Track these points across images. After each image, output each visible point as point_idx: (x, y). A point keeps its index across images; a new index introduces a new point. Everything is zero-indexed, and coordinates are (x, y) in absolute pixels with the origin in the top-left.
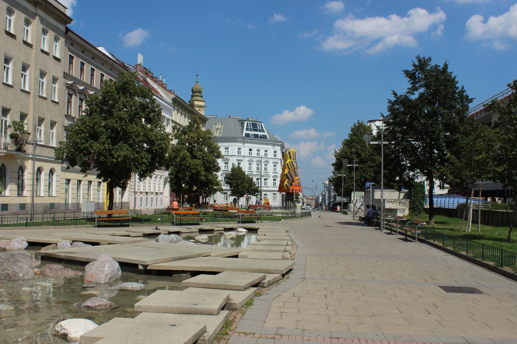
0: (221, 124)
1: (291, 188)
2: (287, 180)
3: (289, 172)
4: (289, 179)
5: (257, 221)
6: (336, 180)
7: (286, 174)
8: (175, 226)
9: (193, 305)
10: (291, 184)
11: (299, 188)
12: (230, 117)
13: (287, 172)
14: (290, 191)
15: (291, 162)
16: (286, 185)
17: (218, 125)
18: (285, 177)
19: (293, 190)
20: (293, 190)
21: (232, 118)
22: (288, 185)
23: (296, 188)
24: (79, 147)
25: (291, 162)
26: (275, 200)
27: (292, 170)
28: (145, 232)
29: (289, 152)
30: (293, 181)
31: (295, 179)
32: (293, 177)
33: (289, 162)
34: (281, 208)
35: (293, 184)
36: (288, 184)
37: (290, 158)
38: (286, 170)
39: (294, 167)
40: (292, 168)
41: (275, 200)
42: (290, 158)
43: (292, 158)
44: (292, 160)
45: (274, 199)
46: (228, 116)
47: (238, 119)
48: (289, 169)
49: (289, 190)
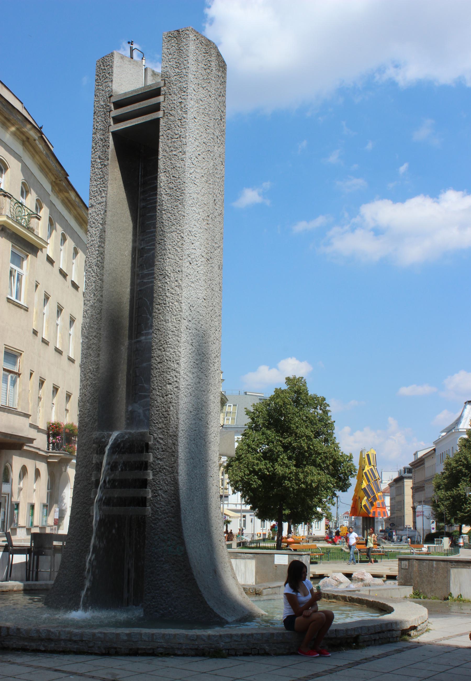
0: (234, 405)
1: (372, 511)
2: (366, 498)
3: (369, 486)
4: (369, 496)
5: (379, 560)
6: (451, 500)
7: (365, 488)
8: (359, 563)
9: (429, 651)
10: (372, 504)
11: (383, 510)
12: (246, 393)
13: (366, 485)
14: (371, 515)
15: (371, 469)
16: (365, 506)
17: (229, 406)
18: (362, 493)
19: (374, 512)
20: (374, 512)
21: (249, 395)
22: (368, 506)
23: (378, 510)
24: (254, 469)
25: (371, 469)
26: (318, 527)
27: (373, 482)
28: (315, 572)
29: (368, 455)
30: (375, 499)
31: (377, 496)
32: (374, 493)
33: (368, 470)
34: (325, 540)
35: (374, 503)
36: (368, 503)
37: (370, 463)
38: (364, 482)
39: (375, 477)
40: (372, 480)
41: (318, 527)
42: (370, 463)
43: (372, 465)
44: (372, 467)
45: (317, 527)
46: (242, 393)
47: (259, 396)
48: (369, 481)
49: (369, 512)
